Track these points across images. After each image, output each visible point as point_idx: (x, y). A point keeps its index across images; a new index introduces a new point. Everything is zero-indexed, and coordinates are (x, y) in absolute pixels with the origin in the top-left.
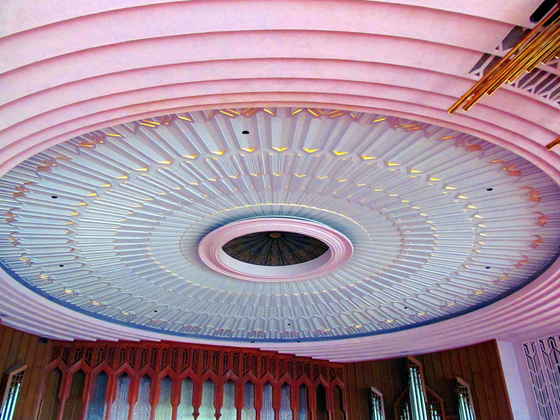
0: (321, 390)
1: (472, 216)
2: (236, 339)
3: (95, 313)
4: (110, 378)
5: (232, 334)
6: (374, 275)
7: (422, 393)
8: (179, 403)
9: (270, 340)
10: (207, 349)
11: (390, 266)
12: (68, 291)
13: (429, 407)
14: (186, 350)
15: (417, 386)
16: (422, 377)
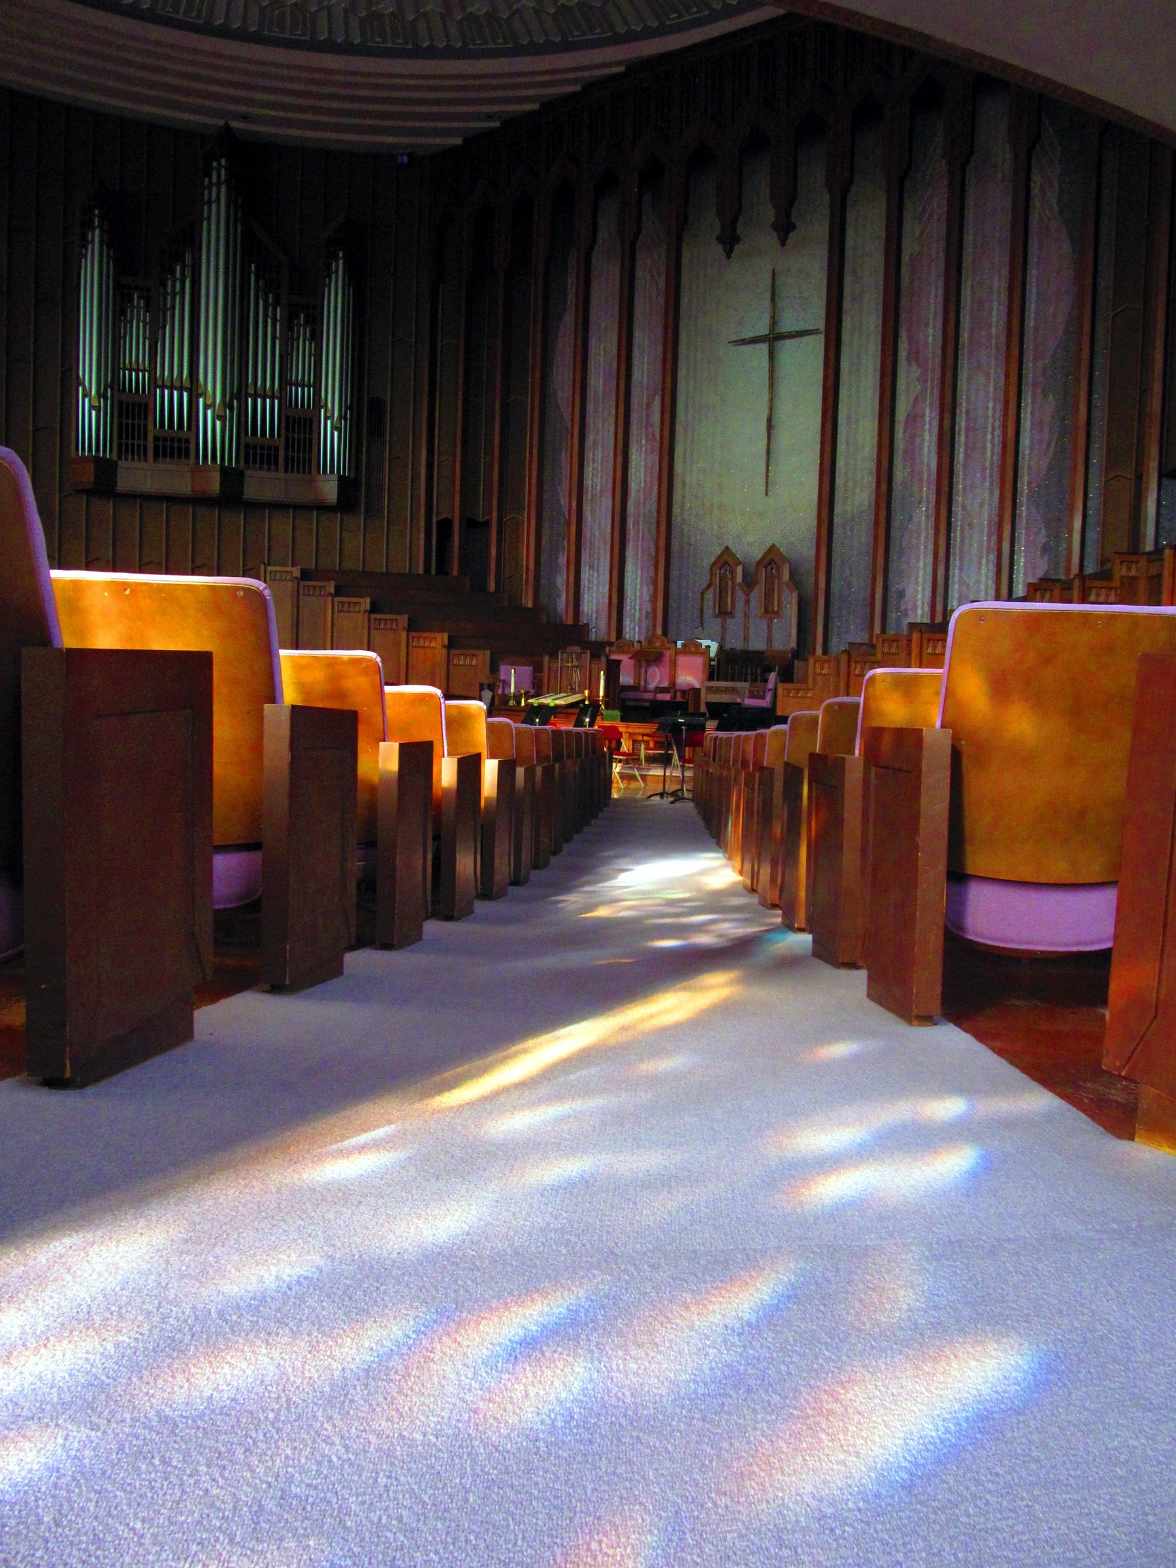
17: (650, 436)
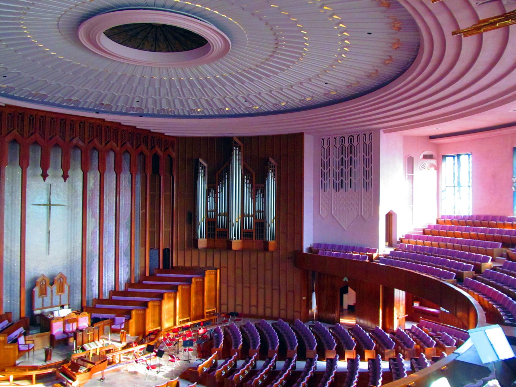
0: (156, 158)
1: (341, 33)
5: (111, 108)
8: (28, 165)
13: (244, 177)
14: (32, 116)
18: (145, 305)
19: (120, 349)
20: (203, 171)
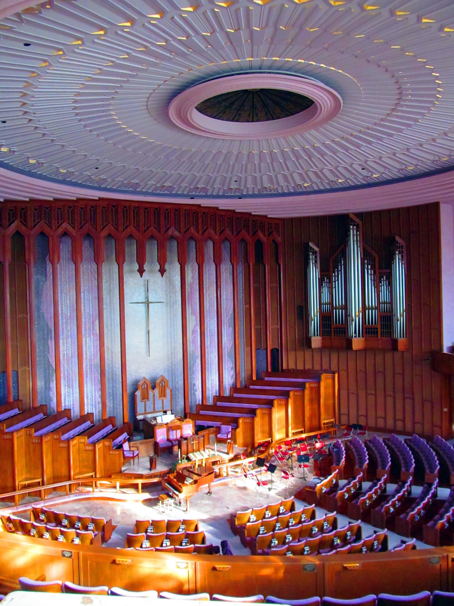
0: (259, 244)
2: (141, 193)
3: (30, 171)
4: (51, 239)
6: (346, 136)
7: (359, 248)
9: (212, 197)
10: (147, 206)
11: (368, 128)
12: (32, 161)
15: (355, 243)
16: (361, 235)
17: (95, 334)
18: (253, 412)
19: (227, 461)
20: (314, 257)
